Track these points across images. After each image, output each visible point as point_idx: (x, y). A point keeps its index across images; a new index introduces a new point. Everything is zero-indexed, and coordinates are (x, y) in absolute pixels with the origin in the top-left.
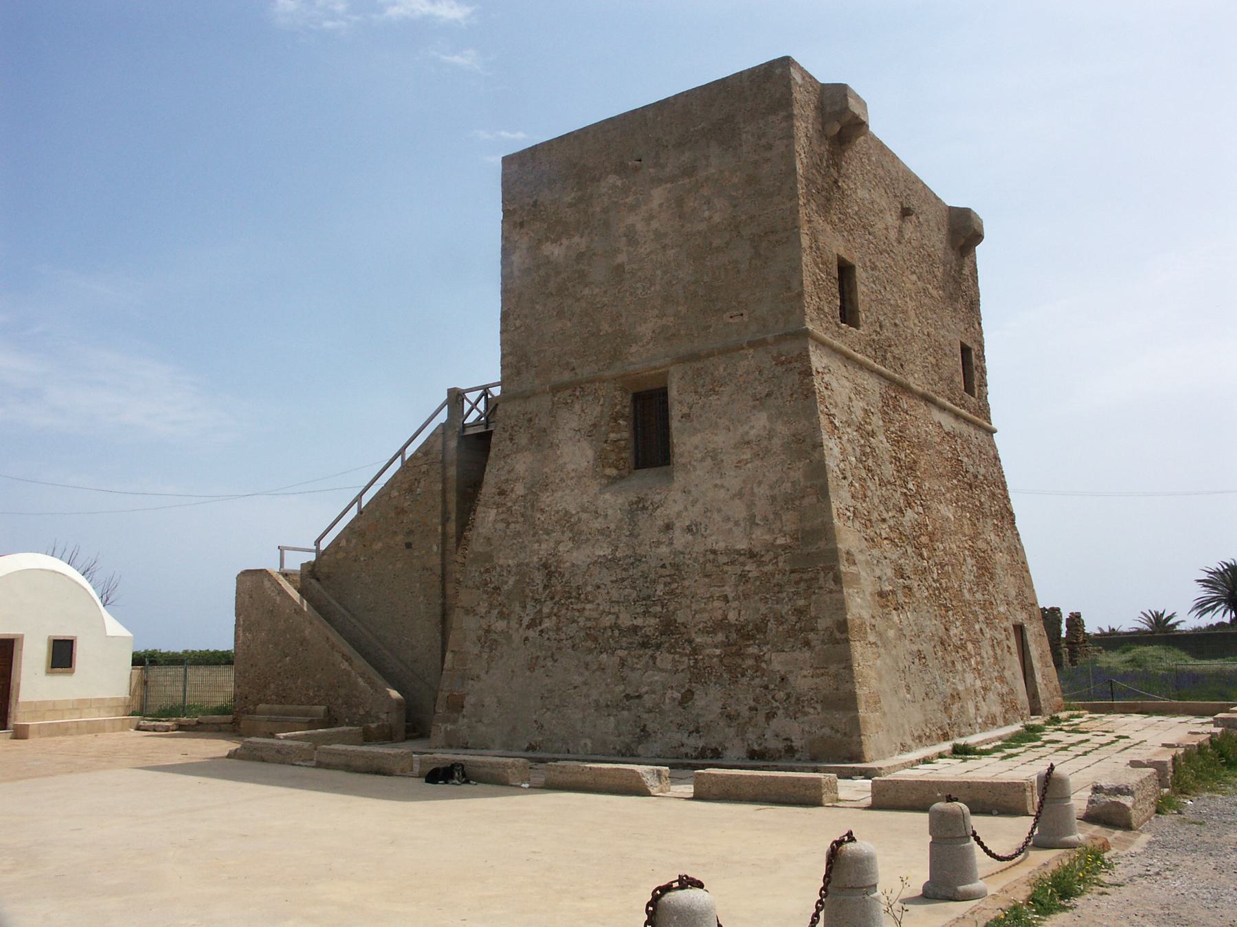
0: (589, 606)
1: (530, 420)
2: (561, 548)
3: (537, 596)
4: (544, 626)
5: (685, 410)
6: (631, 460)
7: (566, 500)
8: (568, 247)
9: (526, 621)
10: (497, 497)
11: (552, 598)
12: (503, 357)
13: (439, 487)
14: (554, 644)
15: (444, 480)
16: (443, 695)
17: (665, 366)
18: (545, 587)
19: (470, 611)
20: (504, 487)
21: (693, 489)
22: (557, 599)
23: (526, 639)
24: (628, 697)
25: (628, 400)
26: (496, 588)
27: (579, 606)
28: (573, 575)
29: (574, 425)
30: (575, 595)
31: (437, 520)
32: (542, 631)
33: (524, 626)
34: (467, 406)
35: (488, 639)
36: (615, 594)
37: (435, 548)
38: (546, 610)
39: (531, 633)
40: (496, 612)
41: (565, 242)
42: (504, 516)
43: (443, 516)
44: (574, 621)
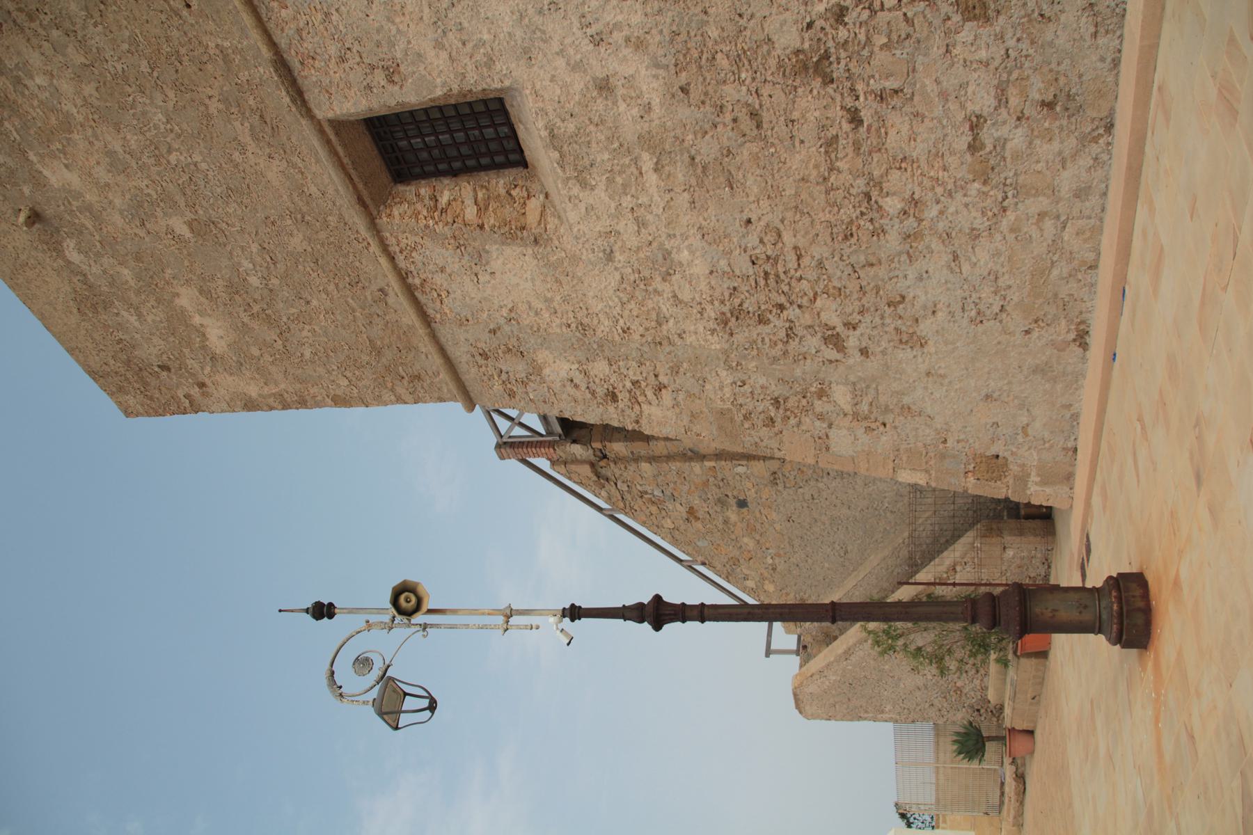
0: (787, 237)
1: (484, 355)
2: (686, 295)
3: (782, 334)
4: (835, 321)
5: (379, 77)
6: (510, 174)
7: (600, 290)
8: (202, 313)
9: (831, 353)
10: (621, 405)
11: (781, 307)
12: (400, 400)
13: (645, 466)
14: (869, 300)
15: (637, 459)
16: (972, 485)
17: (321, 131)
18: (762, 320)
19: (823, 443)
20: (601, 391)
21: (1109, 60)
22: (782, 300)
23: (864, 352)
24: (973, 147)
25: (408, 190)
26: (776, 402)
27: (792, 258)
28: (731, 275)
29: (469, 286)
30: (768, 270)
31: (697, 467)
32: (847, 325)
33: (839, 356)
34: (518, 431)
35: (869, 419)
36: (753, 184)
37: (740, 469)
38: (807, 319)
39: (852, 341)
40: (817, 403)
41: (197, 320)
42: (649, 393)
43: (691, 459)
44: (820, 264)
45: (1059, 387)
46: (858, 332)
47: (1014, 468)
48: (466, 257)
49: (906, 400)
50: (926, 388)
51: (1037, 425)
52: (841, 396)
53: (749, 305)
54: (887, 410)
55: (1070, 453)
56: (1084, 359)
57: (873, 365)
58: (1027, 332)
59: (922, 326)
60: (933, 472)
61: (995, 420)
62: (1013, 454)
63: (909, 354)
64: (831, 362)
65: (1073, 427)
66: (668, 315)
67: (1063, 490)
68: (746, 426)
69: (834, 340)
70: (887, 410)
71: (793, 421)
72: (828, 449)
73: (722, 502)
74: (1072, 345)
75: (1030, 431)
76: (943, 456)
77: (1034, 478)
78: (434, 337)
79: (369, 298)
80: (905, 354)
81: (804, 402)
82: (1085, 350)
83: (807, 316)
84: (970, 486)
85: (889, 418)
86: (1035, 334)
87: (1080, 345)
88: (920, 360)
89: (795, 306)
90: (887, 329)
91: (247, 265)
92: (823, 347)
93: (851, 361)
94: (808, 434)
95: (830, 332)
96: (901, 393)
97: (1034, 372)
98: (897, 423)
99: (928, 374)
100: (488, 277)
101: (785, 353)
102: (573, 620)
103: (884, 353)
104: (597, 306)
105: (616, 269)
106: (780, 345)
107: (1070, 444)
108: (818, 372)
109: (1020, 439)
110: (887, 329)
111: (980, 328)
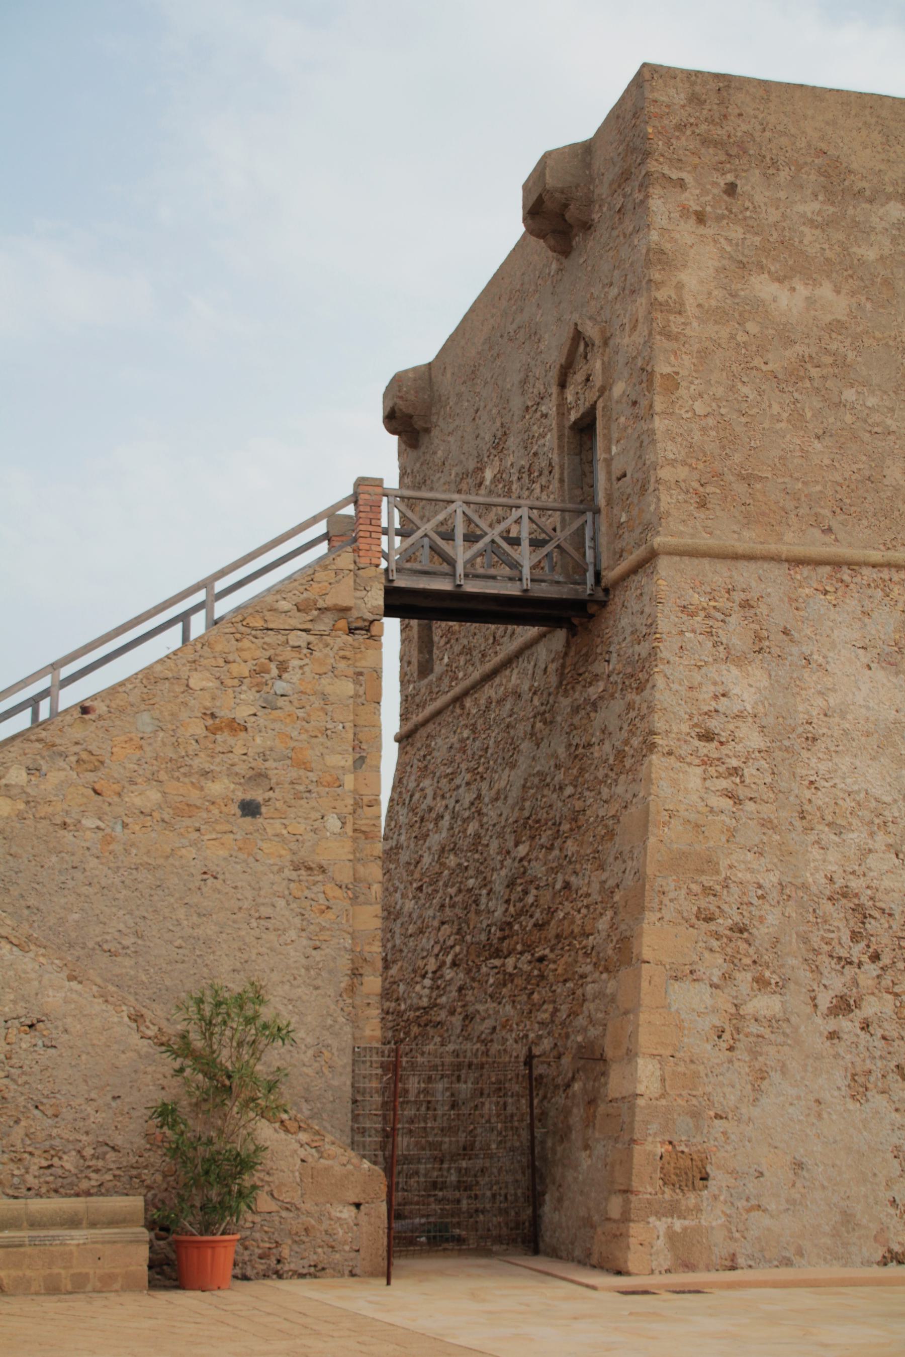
9: (825, 1000)
18: (855, 936)
22: (886, 960)
23: (833, 1035)
45: (829, 1241)
46: (859, 1031)
47: (692, 1199)
48: (887, 649)
49: (776, 1077)
50: (799, 1098)
51: (767, 1221)
52: (765, 1004)
53: (871, 925)
54: (754, 1054)
55: (728, 1263)
56: (868, 1263)
57: (821, 1044)
58: (893, 1202)
59: (879, 1097)
60: (663, 1102)
61: (766, 1173)
62: (715, 1197)
63: (842, 1083)
64: (814, 999)
65: (770, 1261)
66: (844, 836)
67: (665, 1260)
68: (694, 887)
69: (843, 1006)
70: (754, 1054)
71: (715, 944)
72: (676, 978)
73: (258, 777)
74: (885, 1249)
75: (755, 1214)
76: (695, 1115)
77: (678, 1225)
78: (775, 559)
79: (822, 511)
80: (841, 1080)
81: (748, 961)
82: (878, 1263)
83: (870, 982)
84: (649, 1147)
85: (741, 1053)
86: (892, 1211)
87: (884, 1257)
88: (836, 1093)
89: (879, 972)
90: (868, 1061)
91: (871, 401)
92: (832, 993)
93: (819, 1020)
94: (696, 959)
95: (852, 1002)
96: (783, 1069)
97: (844, 1213)
98: (737, 1064)
99: (818, 1102)
100: (865, 661)
101: (816, 952)
102: (381, 480)
103: (837, 1056)
104: (844, 763)
105: (895, 801)
106: (826, 948)
107: (741, 1261)
108: (796, 983)
109: (741, 1204)
110: (868, 1061)
111: (890, 1156)
